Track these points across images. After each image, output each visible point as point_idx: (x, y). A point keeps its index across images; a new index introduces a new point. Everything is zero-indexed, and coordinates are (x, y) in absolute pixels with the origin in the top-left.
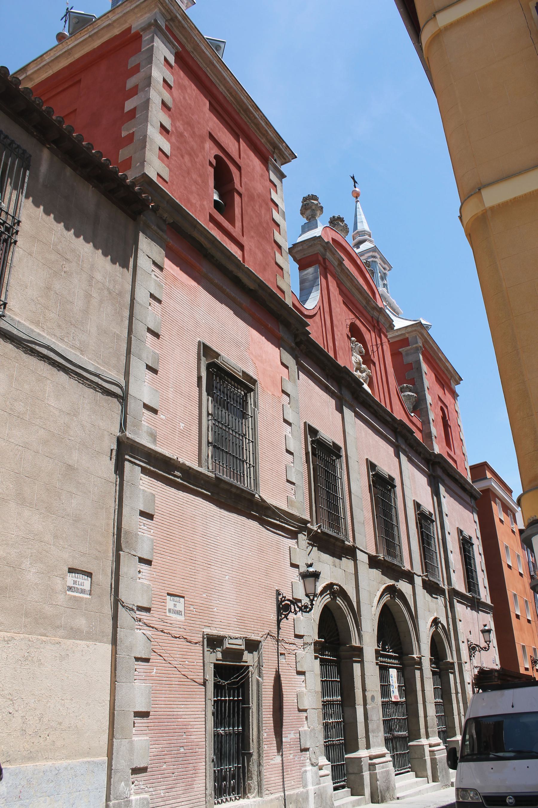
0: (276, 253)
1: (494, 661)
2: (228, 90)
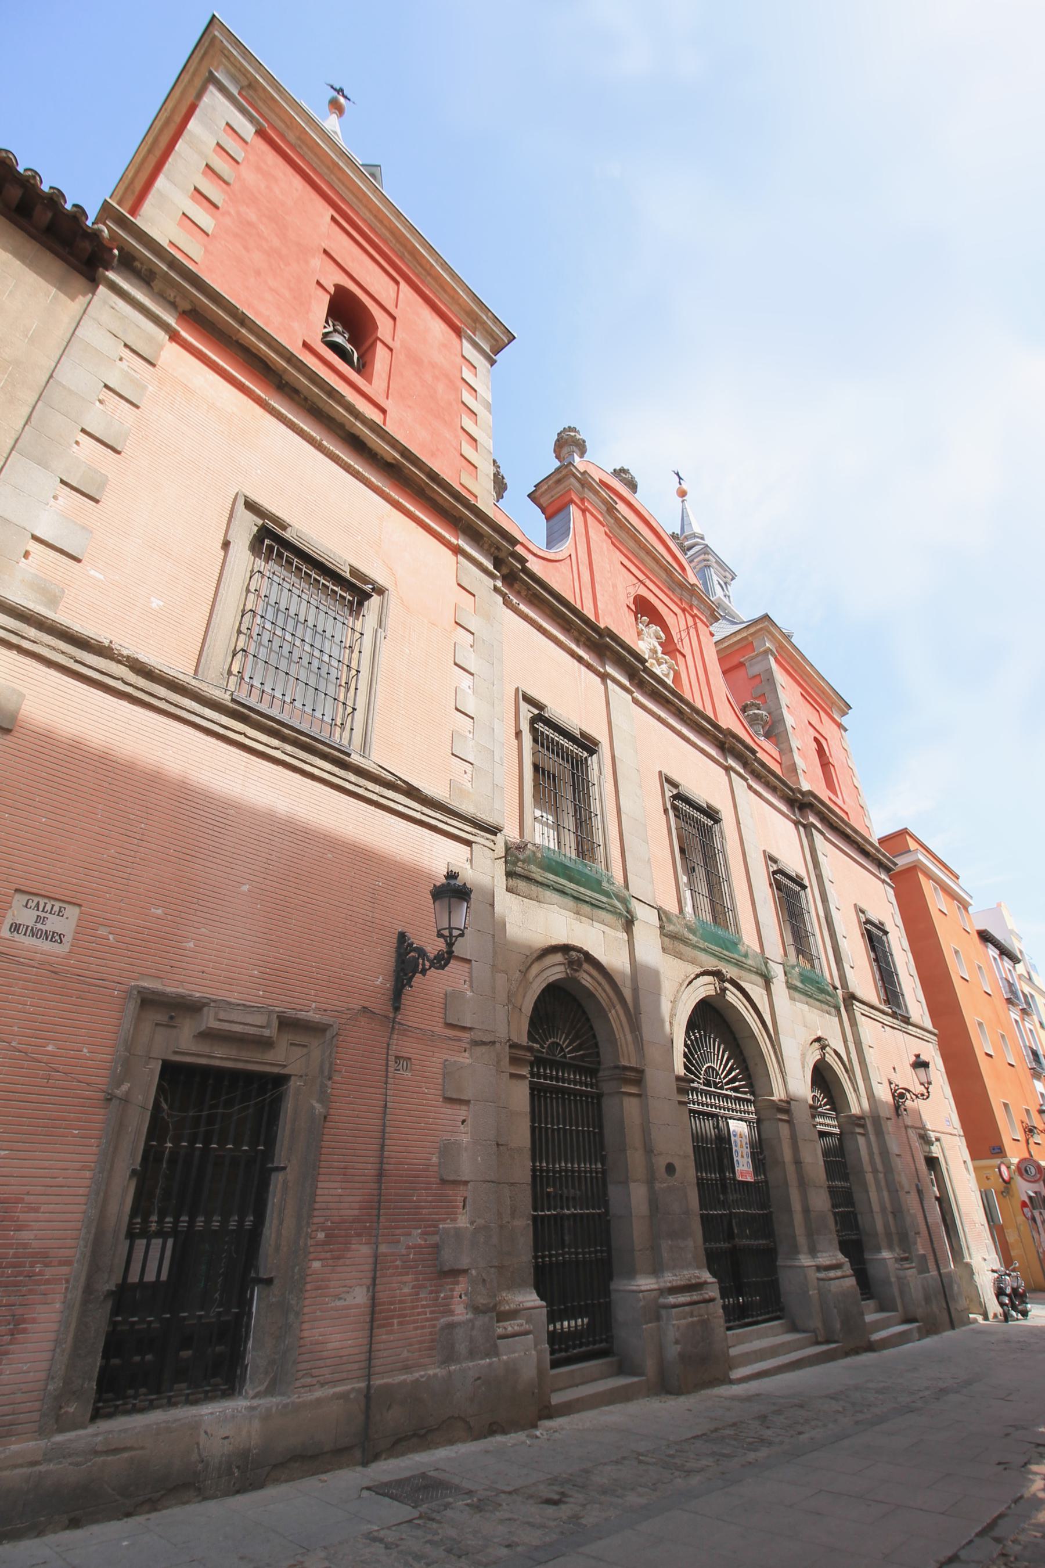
0: (463, 443)
1: (949, 1120)
2: (375, 216)
